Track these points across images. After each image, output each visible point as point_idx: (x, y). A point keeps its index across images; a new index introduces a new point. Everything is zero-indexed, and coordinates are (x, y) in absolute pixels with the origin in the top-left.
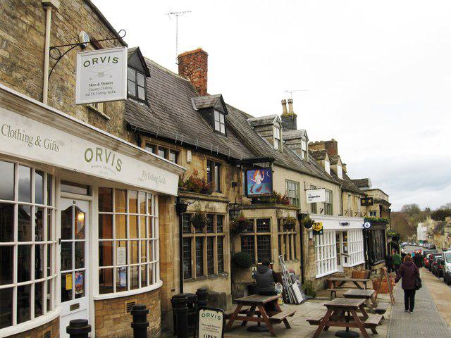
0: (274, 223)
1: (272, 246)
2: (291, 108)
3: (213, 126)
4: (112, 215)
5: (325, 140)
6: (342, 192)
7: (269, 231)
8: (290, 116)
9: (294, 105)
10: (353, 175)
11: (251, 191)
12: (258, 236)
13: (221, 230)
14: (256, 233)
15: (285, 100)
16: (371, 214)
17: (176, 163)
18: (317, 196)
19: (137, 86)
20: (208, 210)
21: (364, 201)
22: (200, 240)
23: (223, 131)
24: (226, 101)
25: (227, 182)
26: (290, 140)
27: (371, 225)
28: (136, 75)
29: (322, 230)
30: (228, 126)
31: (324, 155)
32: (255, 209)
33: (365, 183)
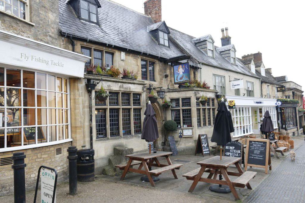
0: (194, 101)
1: (192, 116)
2: (227, 33)
3: (159, 42)
4: (34, 91)
5: (253, 53)
6: (262, 82)
7: (190, 106)
8: (226, 38)
9: (229, 31)
10: (276, 74)
11: (177, 80)
12: (183, 110)
13: (213, 105)
14: (181, 108)
15: (223, 29)
16: (286, 97)
17: (73, 51)
18: (238, 85)
19: (89, 13)
20: (122, 89)
21: (279, 89)
22: (209, 109)
23: (167, 44)
24: (168, 25)
25: (160, 74)
26: (224, 51)
27: (282, 104)
28: (89, 5)
29: (235, 105)
30: (171, 40)
31: (250, 61)
32: (180, 91)
33: (282, 79)
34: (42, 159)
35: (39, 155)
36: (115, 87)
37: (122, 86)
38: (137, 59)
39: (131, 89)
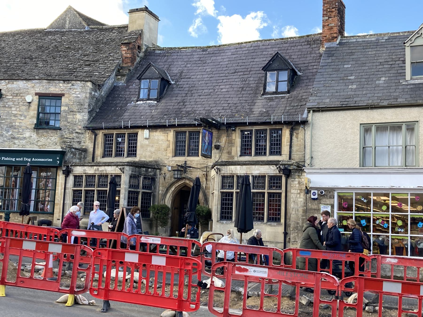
34: (18, 220)
35: (16, 218)
36: (90, 171)
37: (98, 169)
38: (168, 133)
39: (107, 171)
